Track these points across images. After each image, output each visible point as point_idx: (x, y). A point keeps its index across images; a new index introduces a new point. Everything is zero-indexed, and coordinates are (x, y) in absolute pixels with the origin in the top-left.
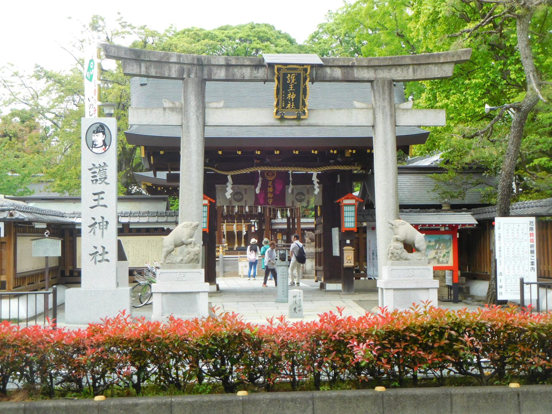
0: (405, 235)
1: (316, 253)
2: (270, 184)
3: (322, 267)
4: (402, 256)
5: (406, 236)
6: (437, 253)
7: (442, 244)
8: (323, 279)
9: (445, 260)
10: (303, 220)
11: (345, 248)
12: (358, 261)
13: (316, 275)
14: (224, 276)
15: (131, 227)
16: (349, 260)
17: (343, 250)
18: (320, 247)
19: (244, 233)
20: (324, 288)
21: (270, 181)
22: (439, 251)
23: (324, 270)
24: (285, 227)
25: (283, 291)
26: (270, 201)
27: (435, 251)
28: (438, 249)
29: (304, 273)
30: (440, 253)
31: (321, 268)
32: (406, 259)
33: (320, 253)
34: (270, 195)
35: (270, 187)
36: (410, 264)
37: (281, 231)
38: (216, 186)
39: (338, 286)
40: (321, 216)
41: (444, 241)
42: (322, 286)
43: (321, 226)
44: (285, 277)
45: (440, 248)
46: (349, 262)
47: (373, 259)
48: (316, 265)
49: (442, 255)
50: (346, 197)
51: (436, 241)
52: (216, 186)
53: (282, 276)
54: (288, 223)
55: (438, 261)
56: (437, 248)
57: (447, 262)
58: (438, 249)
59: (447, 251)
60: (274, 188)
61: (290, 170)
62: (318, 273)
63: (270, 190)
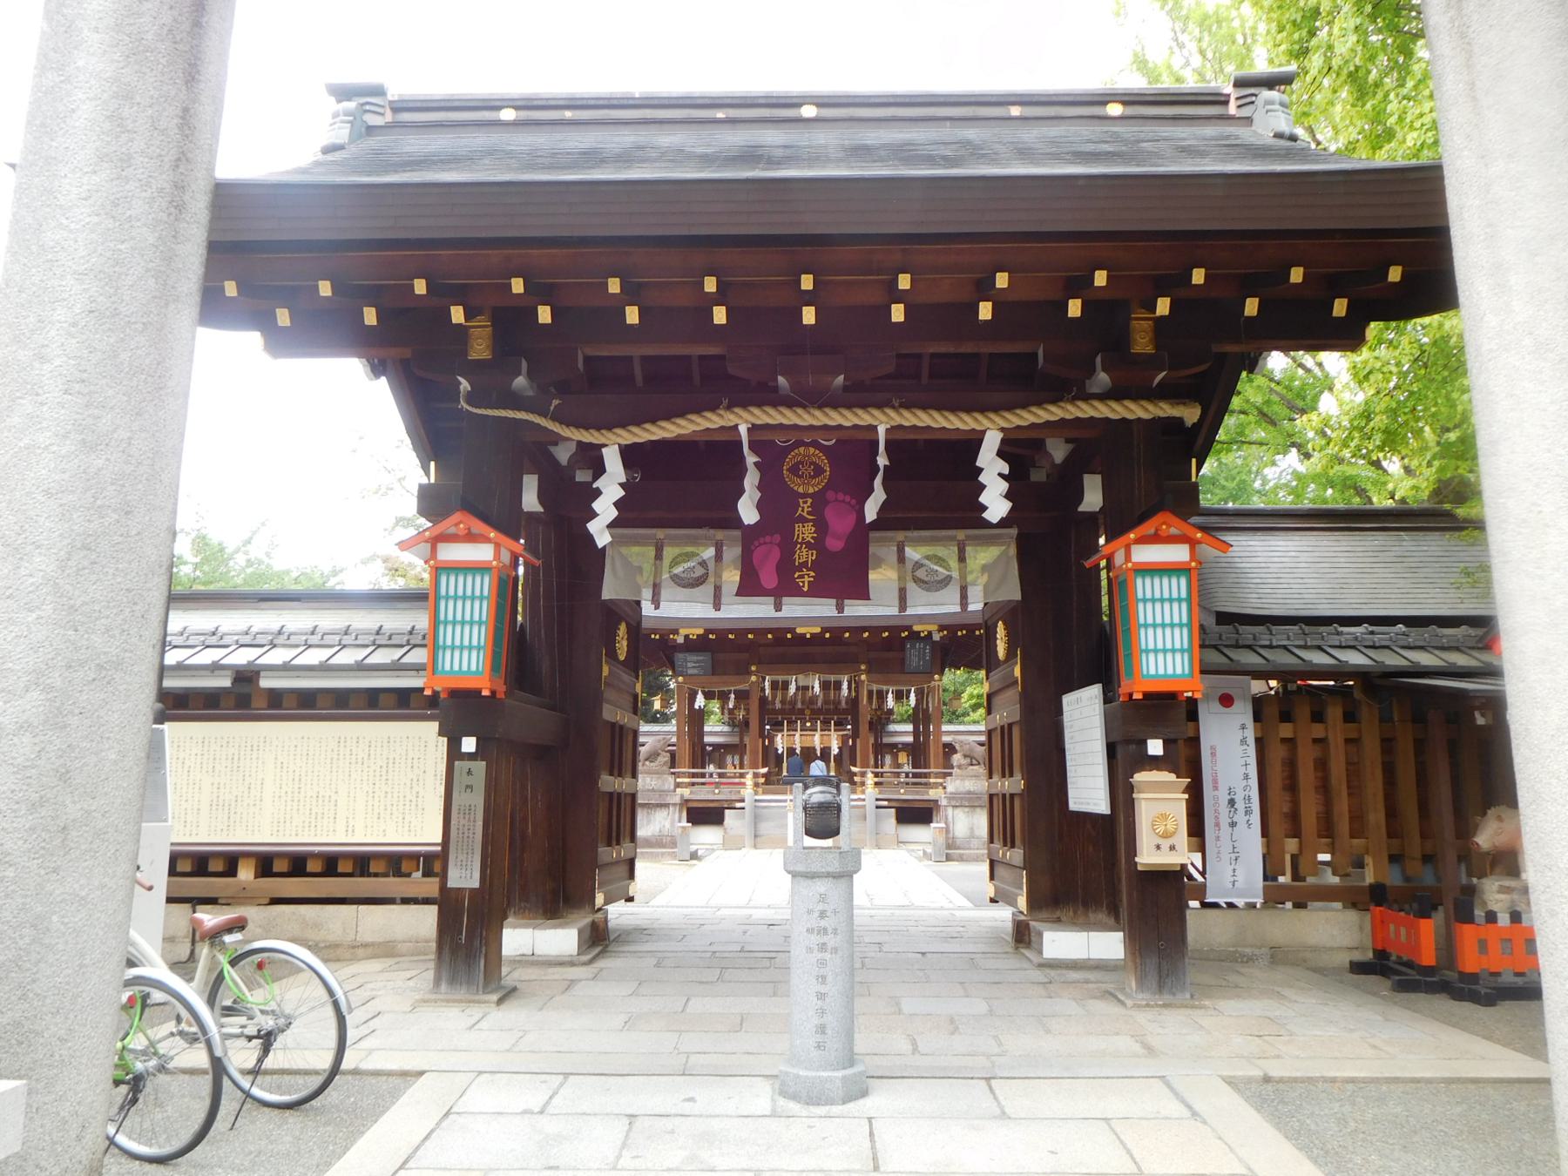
1: (991, 797)
2: (805, 508)
3: (1018, 776)
8: (1022, 902)
10: (945, 728)
11: (1140, 777)
13: (992, 878)
14: (755, 847)
15: (265, 683)
16: (1166, 836)
17: (1131, 788)
18: (1007, 771)
19: (835, 751)
20: (1028, 945)
21: (805, 496)
23: (1028, 865)
24: (910, 739)
25: (822, 1029)
26: (806, 579)
29: (949, 847)
31: (1016, 855)
33: (1008, 799)
34: (804, 555)
35: (803, 520)
37: (905, 746)
39: (1109, 944)
40: (1010, 654)
42: (1022, 935)
43: (1013, 695)
44: (831, 940)
46: (1165, 844)
47: (1233, 825)
48: (991, 840)
50: (1148, 528)
53: (815, 939)
54: (916, 733)
60: (821, 527)
61: (882, 422)
62: (999, 871)
63: (806, 532)
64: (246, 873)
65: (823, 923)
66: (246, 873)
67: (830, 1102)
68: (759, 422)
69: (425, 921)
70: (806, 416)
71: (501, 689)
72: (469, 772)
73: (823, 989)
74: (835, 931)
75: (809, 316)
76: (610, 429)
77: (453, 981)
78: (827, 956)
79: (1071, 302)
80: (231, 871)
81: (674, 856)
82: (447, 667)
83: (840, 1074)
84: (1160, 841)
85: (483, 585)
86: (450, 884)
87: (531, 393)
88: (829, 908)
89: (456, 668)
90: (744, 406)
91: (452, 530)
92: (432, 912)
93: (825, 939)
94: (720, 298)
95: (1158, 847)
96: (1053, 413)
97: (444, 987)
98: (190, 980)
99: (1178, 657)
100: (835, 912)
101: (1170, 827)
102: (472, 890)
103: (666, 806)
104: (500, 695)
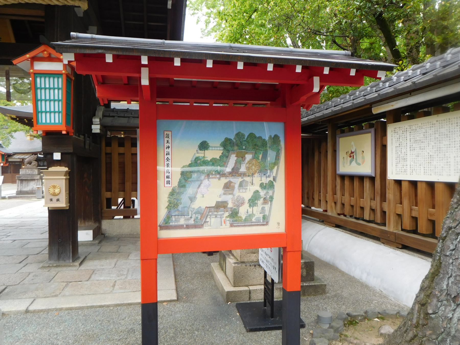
6: (228, 187)
7: (249, 157)
9: (257, 211)
22: (237, 181)
27: (224, 180)
28: (235, 172)
41: (256, 144)
45: (243, 169)
46: (55, 199)
51: (227, 145)
57: (265, 221)
58: (235, 172)
59: (265, 180)
71: (72, 131)
81: (35, 197)
82: (44, 121)
84: (52, 197)
85: (59, 82)
89: (53, 121)
91: (41, 55)
95: (51, 200)
98: (385, 226)
99: (43, 110)
101: (57, 191)
103: (34, 180)
104: (71, 134)
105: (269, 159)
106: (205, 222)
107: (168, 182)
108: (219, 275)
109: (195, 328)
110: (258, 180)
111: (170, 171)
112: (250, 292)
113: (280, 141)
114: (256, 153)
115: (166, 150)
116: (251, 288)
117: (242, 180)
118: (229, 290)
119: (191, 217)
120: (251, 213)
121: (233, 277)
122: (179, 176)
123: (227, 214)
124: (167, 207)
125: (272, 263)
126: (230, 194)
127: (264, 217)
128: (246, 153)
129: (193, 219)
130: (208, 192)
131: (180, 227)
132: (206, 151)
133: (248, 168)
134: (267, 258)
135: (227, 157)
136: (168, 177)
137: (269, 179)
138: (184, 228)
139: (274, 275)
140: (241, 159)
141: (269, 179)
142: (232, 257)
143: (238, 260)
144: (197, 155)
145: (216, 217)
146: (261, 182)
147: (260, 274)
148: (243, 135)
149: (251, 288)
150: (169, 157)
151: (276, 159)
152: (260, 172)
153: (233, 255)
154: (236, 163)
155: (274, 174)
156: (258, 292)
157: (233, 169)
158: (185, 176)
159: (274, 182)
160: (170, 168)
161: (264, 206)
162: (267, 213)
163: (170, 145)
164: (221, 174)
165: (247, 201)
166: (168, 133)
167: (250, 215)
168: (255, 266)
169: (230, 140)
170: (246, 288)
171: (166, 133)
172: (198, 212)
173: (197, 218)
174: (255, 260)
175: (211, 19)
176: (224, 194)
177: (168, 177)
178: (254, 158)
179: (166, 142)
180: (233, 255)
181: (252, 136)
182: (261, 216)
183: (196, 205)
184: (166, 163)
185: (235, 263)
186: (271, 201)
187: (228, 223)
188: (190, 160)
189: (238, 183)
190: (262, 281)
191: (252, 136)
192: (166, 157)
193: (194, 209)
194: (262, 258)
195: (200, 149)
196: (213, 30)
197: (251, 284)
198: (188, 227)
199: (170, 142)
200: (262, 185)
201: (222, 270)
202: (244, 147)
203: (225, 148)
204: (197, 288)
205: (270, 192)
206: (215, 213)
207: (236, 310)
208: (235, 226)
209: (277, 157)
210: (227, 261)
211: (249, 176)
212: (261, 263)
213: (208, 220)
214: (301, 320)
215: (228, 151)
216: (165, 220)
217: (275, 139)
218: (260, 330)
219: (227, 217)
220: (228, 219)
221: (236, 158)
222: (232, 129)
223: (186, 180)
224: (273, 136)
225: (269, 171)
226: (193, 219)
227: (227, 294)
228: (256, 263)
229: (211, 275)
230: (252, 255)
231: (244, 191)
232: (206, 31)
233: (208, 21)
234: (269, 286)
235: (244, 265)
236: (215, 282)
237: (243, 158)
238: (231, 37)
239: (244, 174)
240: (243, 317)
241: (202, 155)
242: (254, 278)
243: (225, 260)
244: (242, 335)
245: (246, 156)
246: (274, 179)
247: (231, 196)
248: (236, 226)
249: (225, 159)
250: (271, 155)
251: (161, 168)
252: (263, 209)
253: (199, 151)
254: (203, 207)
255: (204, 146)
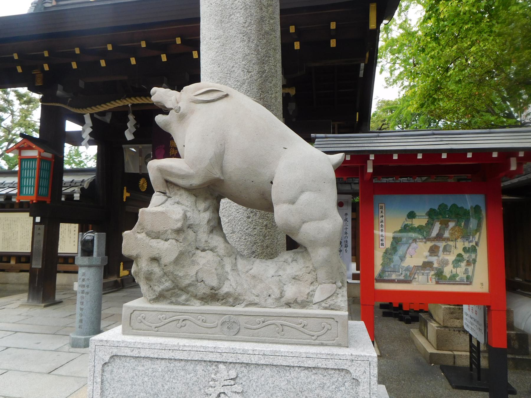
0: (210, 152)
4: (187, 274)
5: (219, 158)
6: (433, 251)
7: (452, 224)
9: (460, 271)
12: (355, 255)
22: (441, 245)
27: (429, 244)
28: (439, 237)
30: (445, 249)
32: (213, 297)
36: (232, 329)
38: (66, 144)
41: (459, 214)
45: (447, 234)
49: (451, 258)
51: (432, 214)
52: (66, 144)
55: (440, 276)
56: (434, 233)
57: (469, 281)
58: (439, 237)
59: (467, 245)
64: (13, 262)
65: (84, 283)
66: (13, 262)
67: (80, 347)
68: (135, 103)
69: (25, 277)
70: (141, 100)
72: (39, 229)
73: (82, 307)
74: (88, 286)
75: (333, 43)
76: (86, 108)
77: (33, 299)
78: (84, 295)
79: (331, 41)
80: (9, 262)
83: (83, 337)
86: (33, 266)
87: (41, 95)
88: (86, 278)
90: (130, 98)
92: (28, 274)
93: (84, 289)
94: (335, 34)
96: (128, 102)
97: (30, 301)
100: (88, 279)
102: (39, 268)
105: (471, 226)
106: (414, 278)
107: (382, 244)
108: (421, 340)
109: (401, 379)
110: (460, 245)
111: (384, 235)
112: (454, 356)
113: (481, 211)
114: (458, 221)
115: (380, 219)
116: (456, 353)
117: (446, 244)
118: (432, 352)
119: (402, 274)
120: (455, 273)
121: (436, 341)
122: (392, 239)
123: (433, 273)
124: (381, 264)
125: (477, 325)
126: (435, 256)
127: (468, 278)
128: (450, 221)
129: (403, 275)
130: (417, 254)
131: (393, 281)
132: (413, 219)
133: (451, 234)
134: (471, 317)
135: (432, 225)
136: (382, 240)
137: (471, 244)
138: (396, 282)
139: (479, 336)
140: (444, 226)
141: (471, 244)
142: (433, 322)
143: (440, 324)
144: (406, 223)
145: (423, 274)
146: (464, 246)
147: (465, 340)
148: (446, 206)
149: (456, 353)
150: (383, 224)
151: (477, 226)
152: (463, 237)
153: (435, 321)
154: (440, 230)
155: (476, 240)
156: (463, 356)
157: (437, 235)
158: (396, 241)
159: (477, 247)
160: (383, 233)
161: (467, 267)
162: (470, 274)
163: (383, 215)
164: (427, 239)
165: (451, 262)
166: (382, 205)
167: (454, 275)
168: (459, 331)
169: (434, 210)
170: (450, 353)
171: (380, 205)
172: (407, 269)
173: (407, 274)
174: (459, 326)
175: (397, 66)
176: (430, 256)
177: (382, 240)
178: (456, 225)
179: (380, 212)
180: (435, 321)
181: (454, 205)
182: (465, 276)
183: (405, 264)
184: (380, 229)
185: (437, 327)
186: (474, 263)
187: (434, 280)
188: (400, 226)
189: (443, 247)
190: (468, 348)
191: (454, 205)
192: (380, 224)
193: (404, 267)
194: (466, 322)
195: (409, 218)
196: (398, 77)
197: (455, 349)
198: (400, 282)
199: (384, 212)
200: (464, 249)
201: (423, 335)
202: (447, 216)
203: (429, 217)
204: (398, 350)
205: (473, 256)
206: (422, 271)
207: (440, 371)
208: (440, 284)
209: (479, 225)
210: (429, 326)
211: (452, 241)
212: (466, 328)
213: (416, 276)
214: (509, 386)
215: (433, 219)
216: (380, 275)
217: (477, 209)
218: (466, 388)
219: (432, 275)
220: (434, 277)
221: (440, 225)
222: (434, 201)
223: (397, 243)
224: (474, 207)
225: (471, 237)
226: (403, 275)
227: (430, 356)
228: (460, 329)
229: (411, 341)
230: (456, 320)
231: (448, 253)
232: (391, 80)
233: (393, 69)
234: (474, 349)
235: (447, 329)
236: (415, 346)
237: (447, 226)
238: (425, 95)
239: (448, 239)
240: (447, 377)
241: (410, 223)
242: (458, 344)
243: (426, 325)
244: (447, 390)
245: (449, 223)
246: (477, 244)
247: (436, 258)
248: (441, 284)
249: (430, 226)
250: (473, 223)
251: (376, 232)
252: (466, 270)
253: (408, 220)
254: (412, 266)
255: (411, 215)
